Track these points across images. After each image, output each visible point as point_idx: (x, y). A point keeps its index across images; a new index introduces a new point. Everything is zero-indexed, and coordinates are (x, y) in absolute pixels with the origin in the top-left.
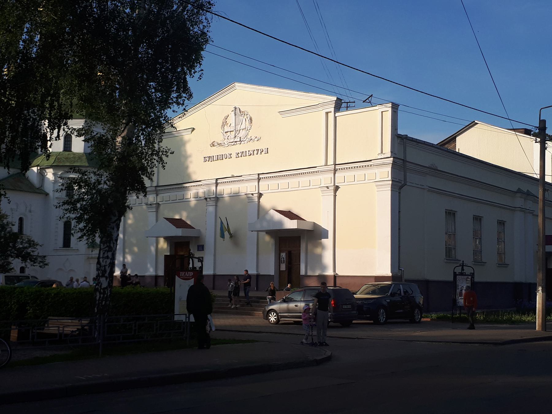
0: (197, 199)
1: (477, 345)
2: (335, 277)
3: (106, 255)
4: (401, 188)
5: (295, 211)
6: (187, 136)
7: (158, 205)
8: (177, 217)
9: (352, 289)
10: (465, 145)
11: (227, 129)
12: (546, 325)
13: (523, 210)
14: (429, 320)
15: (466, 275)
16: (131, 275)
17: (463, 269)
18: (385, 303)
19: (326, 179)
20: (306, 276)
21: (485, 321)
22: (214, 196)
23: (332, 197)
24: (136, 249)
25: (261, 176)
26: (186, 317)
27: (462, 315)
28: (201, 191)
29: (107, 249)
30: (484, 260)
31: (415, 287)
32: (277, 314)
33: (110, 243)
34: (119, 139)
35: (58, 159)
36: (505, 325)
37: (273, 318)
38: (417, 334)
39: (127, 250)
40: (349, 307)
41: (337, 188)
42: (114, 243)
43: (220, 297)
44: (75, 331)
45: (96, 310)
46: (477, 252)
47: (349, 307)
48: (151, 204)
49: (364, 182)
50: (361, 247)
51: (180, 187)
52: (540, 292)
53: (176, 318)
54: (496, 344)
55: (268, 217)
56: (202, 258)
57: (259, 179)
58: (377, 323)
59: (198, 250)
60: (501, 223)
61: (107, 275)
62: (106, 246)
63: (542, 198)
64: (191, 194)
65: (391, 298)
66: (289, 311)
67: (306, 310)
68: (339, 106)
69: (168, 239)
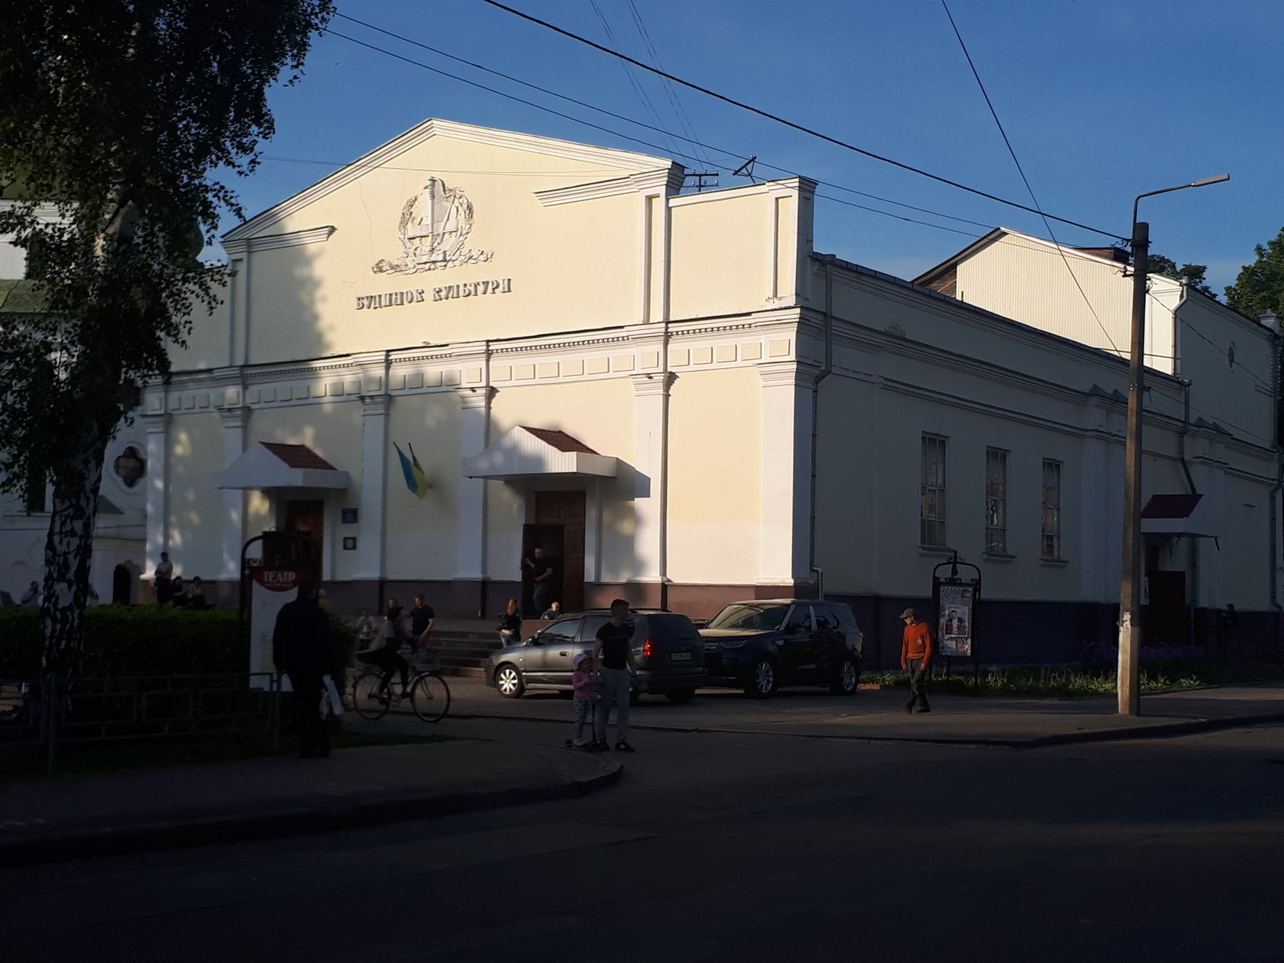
0: (338, 399)
1: (973, 746)
2: (665, 587)
3: (68, 527)
4: (818, 379)
5: (571, 429)
6: (313, 245)
7: (247, 411)
8: (292, 441)
9: (693, 618)
10: (980, 284)
11: (412, 230)
12: (1138, 701)
13: (1101, 435)
14: (876, 687)
15: (961, 585)
16: (184, 578)
17: (954, 572)
18: (771, 648)
19: (647, 355)
20: (599, 586)
21: (1005, 692)
22: (382, 392)
23: (660, 399)
24: (194, 517)
25: (493, 346)
26: (272, 681)
27: (954, 677)
28: (348, 378)
29: (71, 511)
30: (1010, 551)
31: (844, 611)
32: (519, 673)
33: (78, 498)
34: (100, 242)
35: (14, 297)
36: (1048, 702)
37: (508, 683)
38: (843, 719)
39: (173, 519)
40: (687, 656)
41: (671, 378)
42: (88, 499)
43: (444, 634)
44: (10, 713)
45: (44, 662)
46: (995, 534)
47: (687, 656)
48: (229, 410)
49: (734, 364)
50: (723, 520)
51: (300, 368)
52: (1128, 623)
53: (254, 683)
54: (1019, 744)
55: (506, 442)
56: (354, 539)
57: (489, 354)
58: (753, 694)
59: (345, 521)
60: (1052, 466)
61: (71, 575)
62: (67, 504)
63: (1135, 405)
64: (326, 383)
65: (789, 637)
66: (546, 666)
67: (584, 665)
68: (676, 183)
69: (270, 493)
